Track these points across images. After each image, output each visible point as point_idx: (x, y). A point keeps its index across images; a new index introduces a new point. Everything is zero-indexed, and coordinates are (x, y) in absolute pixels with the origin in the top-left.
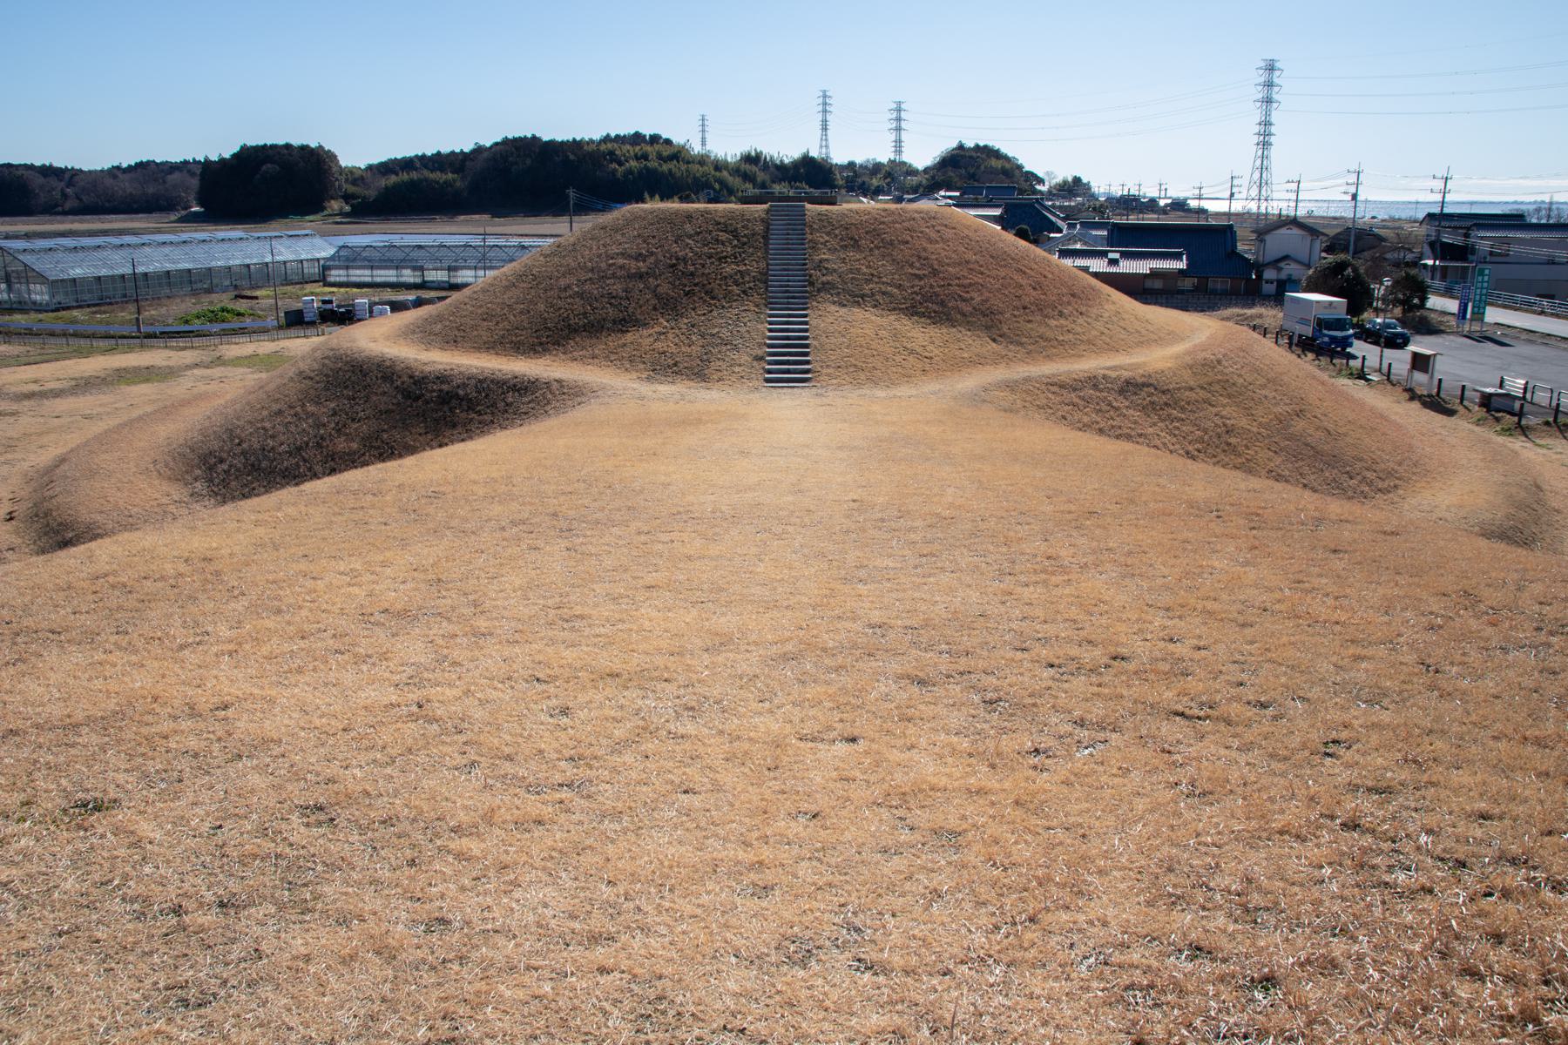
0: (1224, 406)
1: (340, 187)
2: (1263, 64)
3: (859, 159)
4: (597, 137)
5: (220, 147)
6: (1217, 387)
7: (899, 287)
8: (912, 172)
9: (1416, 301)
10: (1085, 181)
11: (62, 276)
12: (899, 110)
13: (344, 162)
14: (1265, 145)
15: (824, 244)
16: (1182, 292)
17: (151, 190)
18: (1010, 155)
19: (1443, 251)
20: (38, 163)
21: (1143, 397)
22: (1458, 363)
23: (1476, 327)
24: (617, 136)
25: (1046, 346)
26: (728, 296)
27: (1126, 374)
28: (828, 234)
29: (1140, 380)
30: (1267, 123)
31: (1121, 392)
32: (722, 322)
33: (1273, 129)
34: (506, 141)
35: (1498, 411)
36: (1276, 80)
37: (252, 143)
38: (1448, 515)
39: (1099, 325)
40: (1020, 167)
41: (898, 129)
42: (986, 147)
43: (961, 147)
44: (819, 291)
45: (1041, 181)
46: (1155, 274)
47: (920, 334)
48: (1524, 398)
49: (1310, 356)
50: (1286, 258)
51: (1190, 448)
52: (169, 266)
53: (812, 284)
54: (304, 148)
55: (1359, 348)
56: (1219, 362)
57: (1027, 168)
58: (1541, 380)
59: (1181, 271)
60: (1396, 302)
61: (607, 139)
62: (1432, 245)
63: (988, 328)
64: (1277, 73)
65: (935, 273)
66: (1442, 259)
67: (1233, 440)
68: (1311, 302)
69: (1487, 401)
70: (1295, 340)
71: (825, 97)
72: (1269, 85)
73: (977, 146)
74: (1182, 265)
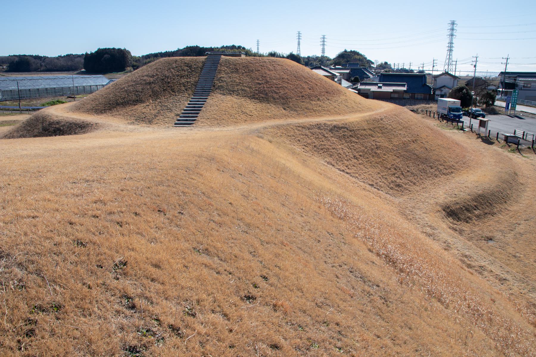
0: (378, 137)
1: (131, 63)
2: (450, 22)
3: (311, 55)
4: (219, 46)
5: (92, 49)
6: (378, 129)
7: (250, 88)
8: (329, 60)
9: (491, 102)
10: (389, 63)
11: (6, 89)
12: (324, 38)
13: (133, 54)
14: (451, 50)
15: (224, 71)
16: (404, 99)
17: (69, 64)
18: (363, 54)
19: (507, 86)
20: (34, 55)
21: (341, 133)
22: (497, 124)
23: (512, 112)
24: (227, 46)
25: (308, 112)
26: (180, 91)
27: (335, 123)
28: (227, 67)
29: (341, 126)
30: (451, 43)
31: (331, 130)
32: (169, 101)
33: (453, 45)
34: (187, 48)
35: (510, 143)
36: (455, 28)
37: (102, 47)
38: (469, 185)
39: (335, 104)
40: (366, 58)
41: (324, 45)
42: (354, 51)
43: (346, 51)
44: (216, 89)
45: (373, 63)
46: (394, 92)
47: (251, 106)
48: (523, 138)
49: (445, 121)
50: (444, 86)
51: (357, 154)
52: (47, 87)
53: (214, 86)
54: (119, 49)
55: (466, 120)
56: (381, 119)
57: (368, 59)
58: (529, 131)
59: (404, 91)
60: (484, 103)
61: (223, 47)
62: (502, 83)
63: (283, 104)
64: (455, 25)
65: (267, 82)
66: (505, 88)
67: (378, 152)
68: (447, 101)
69: (507, 139)
70: (440, 116)
71: (299, 34)
72: (452, 29)
73: (351, 51)
74: (405, 89)
